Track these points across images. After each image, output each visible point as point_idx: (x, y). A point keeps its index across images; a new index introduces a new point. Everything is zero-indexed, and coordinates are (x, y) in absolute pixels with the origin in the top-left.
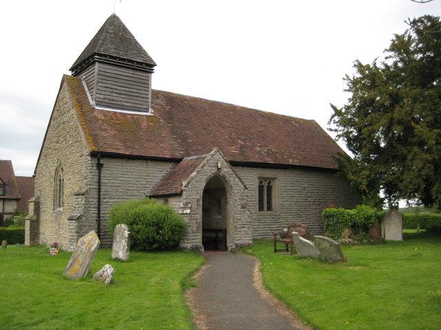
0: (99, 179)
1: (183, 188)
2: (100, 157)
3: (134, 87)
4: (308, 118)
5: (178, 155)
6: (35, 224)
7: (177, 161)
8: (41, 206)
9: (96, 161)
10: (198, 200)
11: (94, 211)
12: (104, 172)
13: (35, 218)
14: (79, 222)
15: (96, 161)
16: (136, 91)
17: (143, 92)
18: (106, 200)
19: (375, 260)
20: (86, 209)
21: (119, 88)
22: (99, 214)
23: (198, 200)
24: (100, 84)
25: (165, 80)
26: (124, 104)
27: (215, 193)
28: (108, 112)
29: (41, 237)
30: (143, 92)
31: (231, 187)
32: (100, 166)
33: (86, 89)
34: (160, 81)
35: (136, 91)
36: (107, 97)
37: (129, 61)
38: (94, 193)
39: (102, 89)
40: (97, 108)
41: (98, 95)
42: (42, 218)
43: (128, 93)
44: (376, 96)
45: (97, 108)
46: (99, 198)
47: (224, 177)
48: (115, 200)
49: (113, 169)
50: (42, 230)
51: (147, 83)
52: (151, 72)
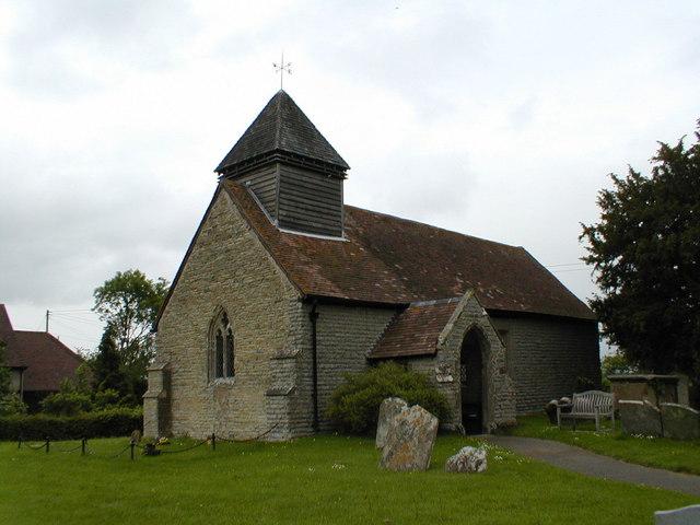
0: (314, 335)
1: (439, 346)
2: (314, 304)
3: (295, 193)
4: (516, 244)
5: (402, 298)
6: (165, 406)
7: (400, 308)
8: (174, 377)
9: (310, 309)
10: (456, 362)
11: (308, 381)
12: (320, 326)
13: (164, 395)
14: (291, 399)
15: (310, 309)
16: (326, 205)
17: (334, 208)
18: (322, 366)
19: (9, 413)
20: (299, 381)
21: (306, 201)
22: (315, 385)
23: (456, 362)
24: (283, 195)
25: (356, 193)
26: (314, 225)
27: (473, 347)
28: (297, 236)
29: (176, 423)
30: (334, 208)
31: (488, 343)
32: (313, 317)
33: (258, 202)
34: (356, 193)
35: (326, 205)
36: (292, 214)
37: (318, 162)
38: (308, 356)
39: (286, 202)
40: (281, 230)
41: (281, 212)
42: (176, 394)
43: (317, 209)
44: (665, 239)
45: (281, 230)
46: (315, 363)
47: (481, 331)
48: (332, 366)
49: (330, 321)
50: (176, 414)
51: (337, 194)
52: (343, 177)
